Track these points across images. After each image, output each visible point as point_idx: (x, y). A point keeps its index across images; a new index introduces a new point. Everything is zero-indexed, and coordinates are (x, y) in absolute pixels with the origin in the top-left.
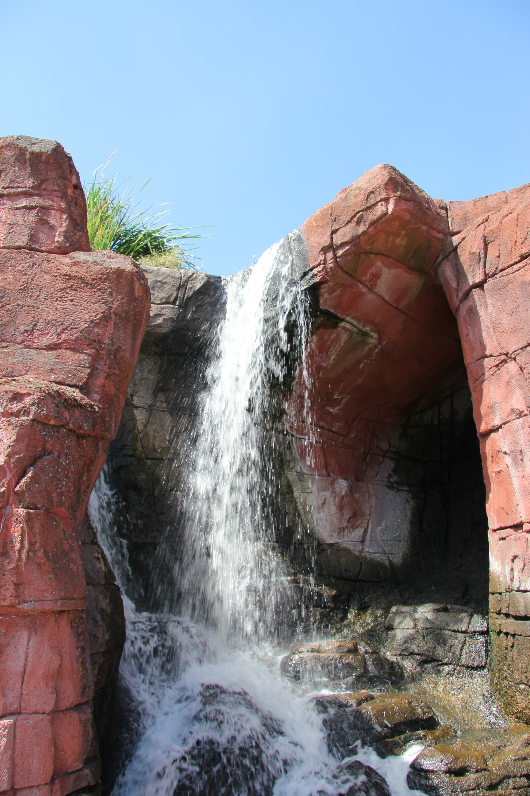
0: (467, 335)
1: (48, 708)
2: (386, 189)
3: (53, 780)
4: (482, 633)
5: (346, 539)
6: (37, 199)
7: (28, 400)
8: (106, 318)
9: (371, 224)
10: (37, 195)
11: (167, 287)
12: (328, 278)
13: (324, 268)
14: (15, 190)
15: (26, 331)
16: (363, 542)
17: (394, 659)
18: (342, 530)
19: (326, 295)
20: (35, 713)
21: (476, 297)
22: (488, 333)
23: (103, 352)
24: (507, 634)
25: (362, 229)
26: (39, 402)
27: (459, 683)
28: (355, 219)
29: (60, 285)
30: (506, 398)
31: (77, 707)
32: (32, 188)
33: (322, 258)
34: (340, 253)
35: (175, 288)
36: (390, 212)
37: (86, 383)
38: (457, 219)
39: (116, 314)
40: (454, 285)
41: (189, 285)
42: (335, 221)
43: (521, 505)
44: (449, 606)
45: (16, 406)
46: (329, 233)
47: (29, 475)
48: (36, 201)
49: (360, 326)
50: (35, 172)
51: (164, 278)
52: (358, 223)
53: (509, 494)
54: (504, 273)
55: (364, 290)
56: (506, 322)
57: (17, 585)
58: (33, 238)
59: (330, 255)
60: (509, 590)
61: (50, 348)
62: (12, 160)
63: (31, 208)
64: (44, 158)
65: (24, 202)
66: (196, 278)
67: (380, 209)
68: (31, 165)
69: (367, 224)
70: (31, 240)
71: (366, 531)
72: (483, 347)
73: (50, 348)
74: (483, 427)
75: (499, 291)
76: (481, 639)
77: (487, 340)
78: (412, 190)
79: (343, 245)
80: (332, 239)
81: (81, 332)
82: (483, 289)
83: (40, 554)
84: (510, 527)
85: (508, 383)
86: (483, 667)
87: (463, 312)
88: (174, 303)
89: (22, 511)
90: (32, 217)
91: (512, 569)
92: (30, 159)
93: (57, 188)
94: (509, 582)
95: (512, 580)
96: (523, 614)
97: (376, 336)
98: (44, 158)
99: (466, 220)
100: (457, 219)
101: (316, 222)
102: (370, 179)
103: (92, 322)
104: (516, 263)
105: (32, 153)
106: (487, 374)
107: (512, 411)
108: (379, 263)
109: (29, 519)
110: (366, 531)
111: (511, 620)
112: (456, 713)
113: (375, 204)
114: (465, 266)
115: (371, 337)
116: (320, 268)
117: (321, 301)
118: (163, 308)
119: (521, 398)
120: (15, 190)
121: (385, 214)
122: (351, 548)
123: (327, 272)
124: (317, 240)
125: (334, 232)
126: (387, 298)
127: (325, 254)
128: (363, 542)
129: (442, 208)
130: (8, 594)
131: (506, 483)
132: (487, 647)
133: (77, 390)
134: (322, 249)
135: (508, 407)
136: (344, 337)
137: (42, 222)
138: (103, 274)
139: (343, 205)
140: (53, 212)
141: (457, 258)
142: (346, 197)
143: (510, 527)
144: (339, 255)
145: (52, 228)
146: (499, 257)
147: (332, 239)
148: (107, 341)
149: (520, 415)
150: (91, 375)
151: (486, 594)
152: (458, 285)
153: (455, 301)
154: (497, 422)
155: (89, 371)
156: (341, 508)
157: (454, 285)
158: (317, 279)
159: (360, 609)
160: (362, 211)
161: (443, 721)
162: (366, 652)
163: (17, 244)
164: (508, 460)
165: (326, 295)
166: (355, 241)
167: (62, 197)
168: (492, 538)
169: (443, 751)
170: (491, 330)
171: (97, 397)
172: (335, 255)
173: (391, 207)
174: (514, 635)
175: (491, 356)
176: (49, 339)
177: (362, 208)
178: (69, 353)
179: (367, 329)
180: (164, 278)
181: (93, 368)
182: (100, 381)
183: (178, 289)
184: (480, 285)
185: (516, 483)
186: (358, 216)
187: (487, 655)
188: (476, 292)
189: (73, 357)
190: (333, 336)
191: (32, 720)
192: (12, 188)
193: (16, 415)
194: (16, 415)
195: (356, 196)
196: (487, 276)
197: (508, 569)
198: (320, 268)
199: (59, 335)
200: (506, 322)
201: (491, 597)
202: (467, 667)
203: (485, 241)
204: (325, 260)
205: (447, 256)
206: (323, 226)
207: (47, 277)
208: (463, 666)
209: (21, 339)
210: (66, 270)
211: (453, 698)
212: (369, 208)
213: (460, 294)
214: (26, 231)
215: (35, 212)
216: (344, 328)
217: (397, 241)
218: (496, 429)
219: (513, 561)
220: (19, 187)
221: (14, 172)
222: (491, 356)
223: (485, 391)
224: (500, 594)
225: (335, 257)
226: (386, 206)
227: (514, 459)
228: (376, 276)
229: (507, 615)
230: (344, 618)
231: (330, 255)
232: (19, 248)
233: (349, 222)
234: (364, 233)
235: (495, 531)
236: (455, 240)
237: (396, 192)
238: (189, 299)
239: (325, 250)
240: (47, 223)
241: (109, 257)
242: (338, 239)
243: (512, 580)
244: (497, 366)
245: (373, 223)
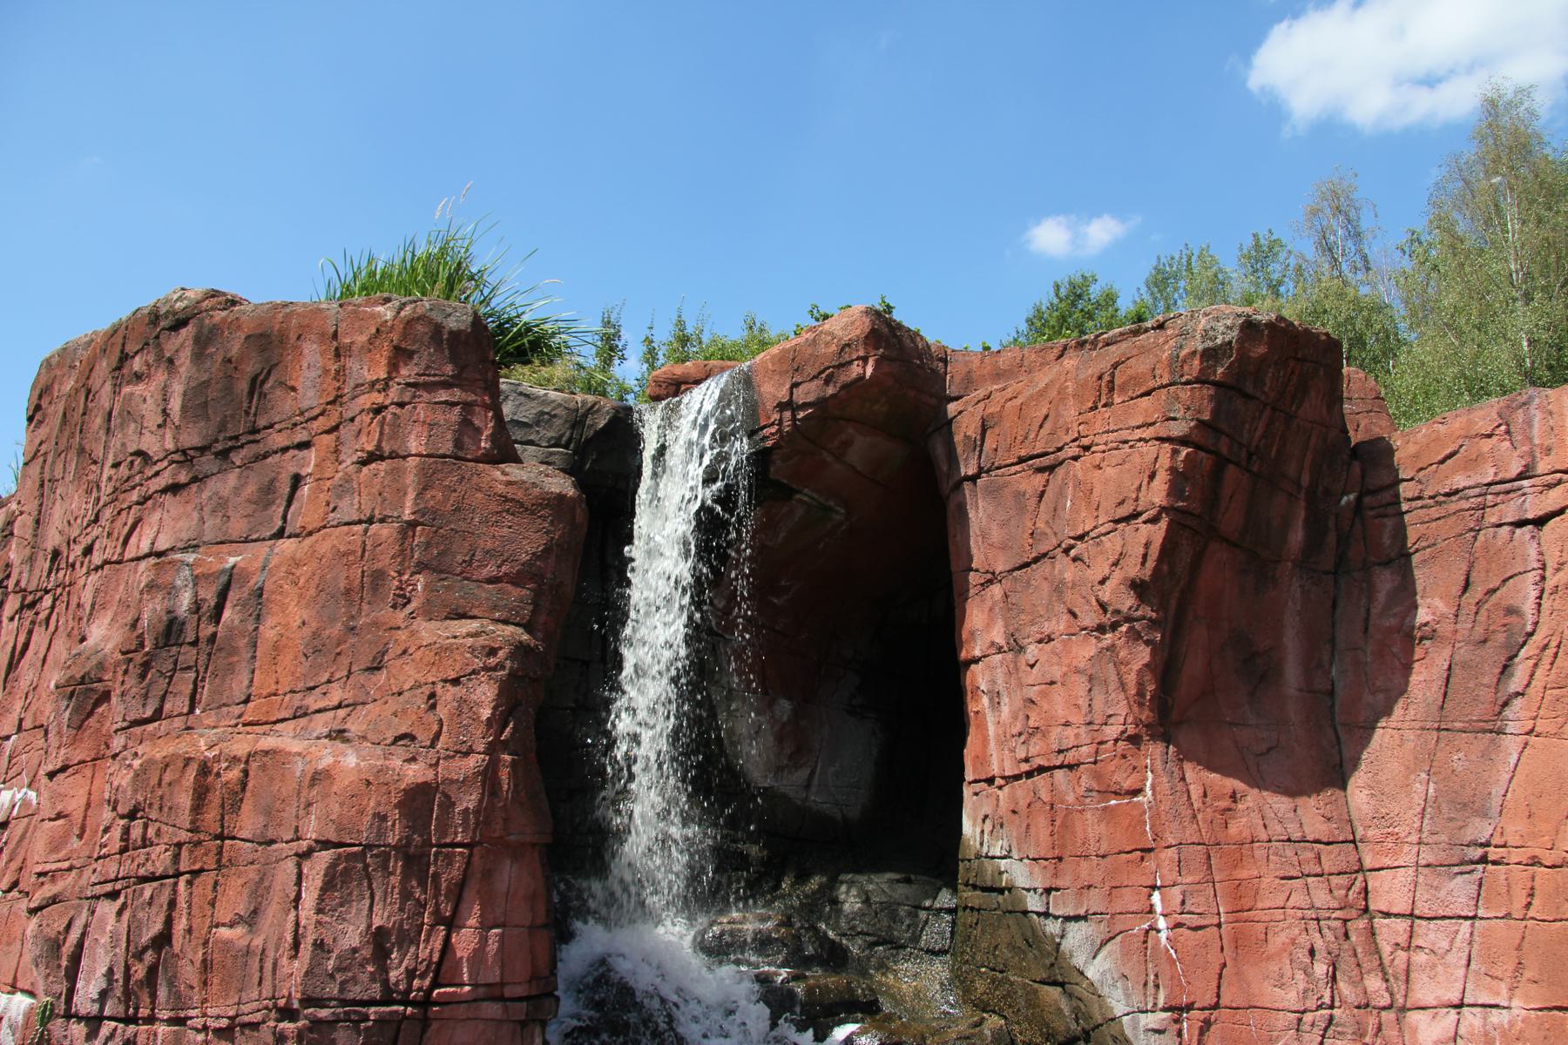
0: (955, 536)
1: (528, 923)
2: (865, 344)
3: (530, 982)
4: (950, 911)
5: (785, 782)
6: (457, 392)
7: (501, 653)
8: (547, 550)
9: (843, 387)
10: (456, 386)
11: (558, 422)
12: (782, 443)
13: (779, 431)
14: (432, 379)
15: (464, 561)
16: (808, 786)
17: (837, 939)
18: (779, 770)
19: (779, 463)
20: (517, 926)
21: (967, 492)
22: (977, 542)
23: (544, 587)
24: (972, 909)
25: (830, 391)
26: (511, 656)
27: (916, 969)
28: (823, 376)
29: (494, 507)
30: (989, 626)
31: (545, 926)
32: (452, 376)
33: (776, 416)
34: (801, 415)
35: (567, 425)
36: (867, 377)
37: (529, 621)
38: (957, 379)
39: (558, 545)
40: (945, 468)
41: (588, 422)
42: (797, 370)
43: (995, 756)
44: (913, 877)
45: (492, 661)
46: (788, 386)
47: (511, 725)
48: (457, 394)
49: (822, 500)
50: (454, 359)
51: (554, 409)
52: (827, 382)
53: (985, 740)
54: (999, 472)
55: (829, 459)
56: (996, 534)
57: (505, 820)
58: (458, 444)
59: (787, 414)
60: (978, 856)
61: (492, 580)
62: (426, 338)
63: (454, 404)
64: (463, 337)
65: (443, 396)
66: (598, 410)
67: (856, 370)
68: (450, 348)
69: (838, 385)
70: (456, 446)
71: (813, 773)
72: (971, 559)
73: (492, 580)
74: (963, 655)
75: (994, 492)
76: (948, 918)
77: (974, 551)
78: (900, 342)
79: (805, 406)
80: (792, 394)
81: (523, 564)
82: (975, 484)
83: (523, 794)
84: (985, 781)
85: (991, 610)
86: (945, 952)
87: (951, 507)
88: (566, 446)
89: (508, 758)
90: (455, 414)
91: (982, 832)
92: (448, 340)
93: (478, 377)
94: (978, 846)
95: (982, 844)
96: (989, 884)
97: (843, 511)
98: (463, 337)
99: (969, 382)
100: (957, 379)
101: (773, 364)
102: (846, 325)
103: (533, 554)
104: (1013, 464)
105: (451, 332)
106: (972, 592)
107: (993, 643)
108: (850, 431)
109: (514, 764)
110: (813, 773)
111: (978, 893)
112: (906, 1002)
113: (850, 362)
114: (959, 450)
115: (837, 512)
116: (773, 430)
117: (772, 470)
118: (552, 454)
119: (1002, 630)
120: (432, 379)
121: (861, 378)
122: (792, 794)
123: (782, 437)
124: (772, 390)
125: (795, 385)
126: (859, 469)
127: (781, 411)
128: (808, 786)
129: (941, 360)
130: (498, 827)
131: (983, 727)
132: (953, 928)
133: (520, 630)
134: (778, 406)
135: (988, 638)
136: (800, 512)
137: (466, 423)
138: (543, 499)
139: (809, 351)
140: (477, 409)
141: (950, 435)
142: (814, 340)
143: (985, 781)
144: (799, 417)
145: (479, 431)
146: (996, 450)
147: (792, 394)
148: (549, 575)
149: (1000, 650)
150: (533, 612)
151: (955, 860)
152: (949, 469)
153: (946, 487)
154: (977, 653)
155: (531, 607)
156: (780, 739)
157: (945, 468)
158: (769, 443)
159: (797, 877)
160: (834, 367)
161: (887, 1007)
162: (802, 927)
163: (441, 452)
164: (985, 700)
165: (779, 463)
166: (820, 404)
167: (485, 389)
168: (967, 792)
169: (879, 1028)
170: (980, 539)
171: (540, 635)
172: (794, 416)
173: (869, 370)
174: (978, 910)
175: (977, 570)
176: (490, 570)
177: (834, 363)
178: (510, 587)
179: (831, 503)
180: (554, 409)
181: (535, 603)
182: (542, 618)
183: (573, 427)
184: (973, 479)
185: (992, 730)
186: (827, 372)
187: (952, 938)
188: (967, 486)
189: (515, 593)
190: (785, 509)
191: (515, 931)
192: (429, 375)
193: (494, 669)
194: (494, 669)
195: (827, 344)
196: (981, 469)
197: (978, 830)
198: (773, 430)
199: (499, 567)
200: (996, 534)
201: (961, 865)
202: (928, 951)
203: (983, 425)
204: (781, 419)
205: (939, 429)
206: (781, 374)
207: (479, 495)
208: (922, 950)
209: (459, 570)
210: (501, 488)
211: (904, 986)
212: (841, 365)
213: (951, 484)
214: (449, 436)
215: (458, 409)
216: (800, 501)
217: (876, 407)
218: (976, 661)
219: (984, 821)
220: (435, 375)
221: (429, 354)
222: (977, 570)
223: (968, 612)
224: (969, 860)
225: (794, 418)
226: (864, 367)
227: (991, 700)
228: (847, 444)
229: (975, 887)
230: (777, 887)
231: (787, 414)
232: (444, 456)
233: (815, 377)
234: (832, 396)
235: (970, 783)
236: (952, 408)
237: (878, 349)
238: (588, 441)
239: (782, 407)
240: (471, 423)
241: (547, 476)
242: (801, 396)
243: (982, 844)
244: (982, 585)
245: (845, 387)
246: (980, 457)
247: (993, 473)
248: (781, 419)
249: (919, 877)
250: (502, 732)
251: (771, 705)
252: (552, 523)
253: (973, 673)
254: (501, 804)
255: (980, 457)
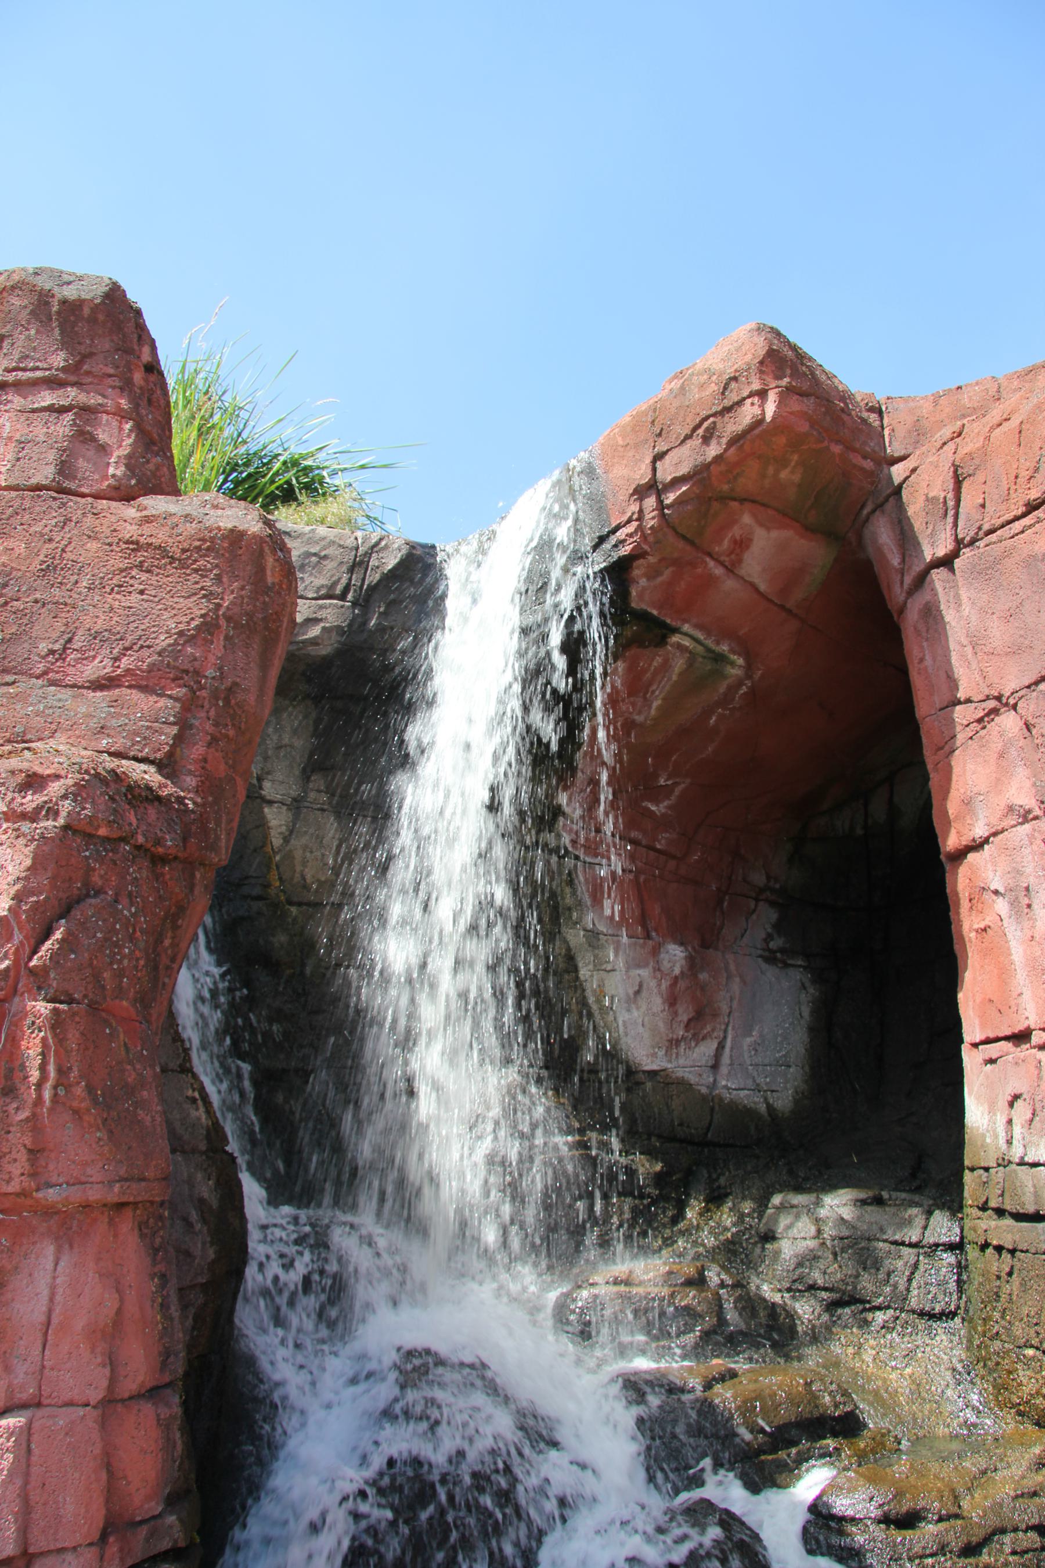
1: (95, 1395)
2: (761, 372)
4: (951, 1247)
5: (681, 1061)
7: (55, 788)
8: (208, 627)
9: (732, 442)
10: (73, 385)
11: (329, 565)
12: (646, 547)
13: (640, 528)
14: (29, 374)
15: (52, 652)
16: (715, 1067)
18: (673, 1043)
19: (643, 582)
20: (70, 1404)
21: (939, 586)
22: (963, 656)
23: (204, 693)
24: (999, 1249)
25: (713, 450)
26: (78, 793)
27: (906, 1345)
28: (701, 431)
29: (118, 562)
30: (998, 784)
31: (153, 1393)
32: (64, 369)
33: (635, 507)
34: (670, 498)
35: (344, 568)
36: (768, 418)
37: (170, 754)
38: (901, 432)
39: (229, 619)
40: (895, 561)
41: (373, 562)
42: (660, 435)
44: (885, 1195)
45: (31, 801)
46: (648, 460)
47: (58, 935)
48: (71, 395)
49: (710, 643)
50: (69, 340)
51: (324, 548)
52: (706, 440)
53: (1004, 973)
54: (993, 537)
55: (718, 571)
56: (998, 634)
57: (34, 1153)
58: (65, 468)
59: (651, 502)
60: (1004, 1163)
61: (98, 685)
62: (24, 314)
63: (62, 410)
64: (86, 311)
65: (47, 398)
66: (386, 547)
67: (749, 412)
68: (61, 326)
69: (724, 441)
70: (61, 472)
71: (721, 1047)
72: (953, 683)
73: (98, 685)
74: (952, 842)
75: (983, 572)
76: (949, 1258)
78: (813, 374)
79: (676, 482)
80: (654, 470)
81: (160, 654)
82: (952, 570)
83: (79, 1090)
84: (1006, 1038)
85: (1001, 755)
86: (952, 1315)
87: (912, 615)
88: (343, 597)
89: (43, 1007)
90: (63, 427)
91: (1010, 1122)
92: (58, 313)
93: (112, 371)
95: (1009, 1142)
96: (1031, 1209)
97: (741, 661)
98: (86, 311)
99: (919, 433)
100: (901, 432)
101: (624, 438)
102: (730, 353)
103: (181, 634)
104: (1017, 518)
105: (64, 302)
106: (961, 737)
107: (1010, 809)
108: (747, 519)
109: (57, 1022)
110: (721, 1047)
111: (1008, 1221)
112: (900, 1405)
113: (740, 403)
114: (918, 525)
115: (732, 664)
116: (630, 528)
117: (634, 593)
118: (321, 607)
119: (1028, 784)
120: (29, 374)
121: (759, 422)
122: (693, 1079)
123: (644, 536)
124: (625, 472)
125: (659, 457)
126: (763, 587)
127: (641, 499)
128: (715, 1067)
129: (871, 410)
130: (16, 1170)
131: (998, 952)
132: (959, 1274)
133: (152, 769)
134: (636, 491)
135: (1000, 803)
136: (679, 664)
137: (83, 436)
139: (676, 403)
140: (105, 417)
141: (901, 508)
142: (682, 388)
143: (1006, 1038)
144: (667, 502)
145: (103, 449)
146: (983, 506)
147: (654, 470)
148: (210, 672)
149: (1026, 817)
150: (179, 739)
151: (958, 1169)
152: (903, 561)
153: (897, 593)
154: (980, 831)
155: (175, 730)
156: (672, 1001)
157: (895, 561)
158: (626, 550)
159: (709, 1200)
160: (714, 415)
161: (873, 1420)
162: (722, 1285)
163: (34, 481)
164: (1001, 906)
165: (643, 582)
166: (700, 475)
167: (122, 389)
168: (971, 1060)
169: (873, 1480)
170: (969, 650)
171: (191, 781)
172: (660, 501)
173: (770, 408)
174: (1013, 1252)
175: (968, 701)
176: (97, 667)
177: (715, 409)
178: (135, 695)
179: (724, 648)
180: (324, 548)
181: (184, 724)
182: (197, 750)
183: (351, 570)
184: (947, 562)
185: (1018, 952)
186: (706, 425)
188: (938, 575)
189: (143, 704)
190: (658, 661)
191: (63, 1418)
192: (24, 370)
193: (32, 817)
194: (32, 817)
195: (702, 386)
196: (959, 544)
197: (1001, 1120)
198: (630, 528)
199: (116, 659)
200: (998, 634)
201: (968, 1177)
202: (922, 1314)
203: (956, 475)
204: (641, 511)
206: (636, 446)
207: (92, 546)
208: (913, 1312)
209: (41, 667)
210: (130, 531)
211: (893, 1376)
212: (728, 410)
213: (908, 580)
214: (52, 456)
215: (69, 417)
216: (679, 646)
217: (784, 475)
218: (977, 846)
219: (1011, 1104)
220: (37, 369)
221: (28, 338)
222: (968, 701)
223: (956, 771)
224: (987, 1169)
225: (661, 506)
226: (762, 406)
227: (1014, 903)
228: (742, 544)
229: (1000, 1212)
231: (651, 502)
232: (38, 488)
233: (688, 437)
234: (718, 459)
235: (975, 1045)
236: (898, 472)
238: (373, 588)
239: (640, 492)
240: (93, 439)
241: (216, 507)
242: (667, 471)
243: (1009, 1142)
244: (980, 720)
245: (735, 440)
246: (955, 525)
247: (981, 544)
248: (641, 511)
249: (894, 1194)
250: (35, 951)
251: (655, 952)
252: (219, 579)
253: (971, 866)
254: (23, 1115)
255: (955, 525)
